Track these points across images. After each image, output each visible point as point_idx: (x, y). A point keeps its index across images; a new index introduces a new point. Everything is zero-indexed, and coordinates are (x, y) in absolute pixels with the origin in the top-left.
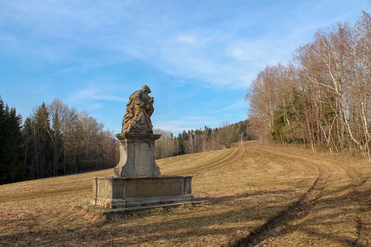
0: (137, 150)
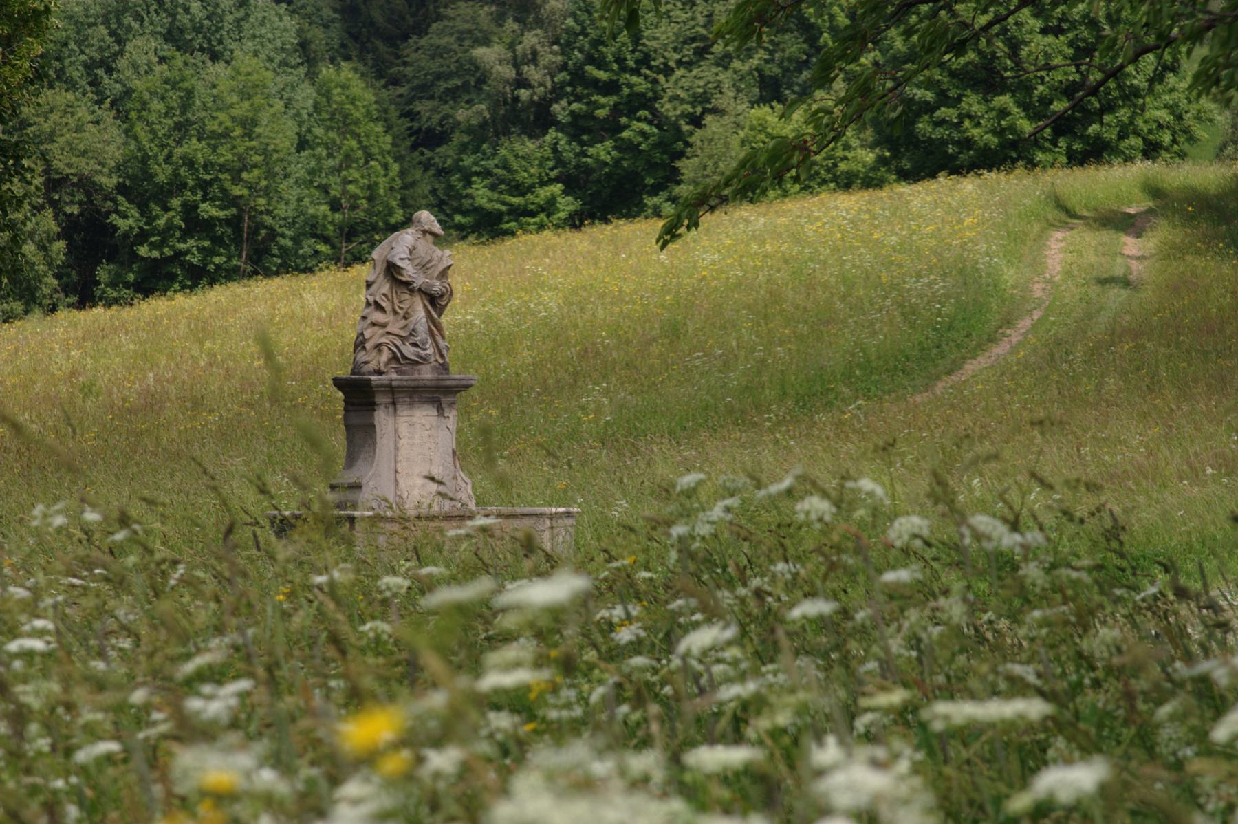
0: (403, 429)
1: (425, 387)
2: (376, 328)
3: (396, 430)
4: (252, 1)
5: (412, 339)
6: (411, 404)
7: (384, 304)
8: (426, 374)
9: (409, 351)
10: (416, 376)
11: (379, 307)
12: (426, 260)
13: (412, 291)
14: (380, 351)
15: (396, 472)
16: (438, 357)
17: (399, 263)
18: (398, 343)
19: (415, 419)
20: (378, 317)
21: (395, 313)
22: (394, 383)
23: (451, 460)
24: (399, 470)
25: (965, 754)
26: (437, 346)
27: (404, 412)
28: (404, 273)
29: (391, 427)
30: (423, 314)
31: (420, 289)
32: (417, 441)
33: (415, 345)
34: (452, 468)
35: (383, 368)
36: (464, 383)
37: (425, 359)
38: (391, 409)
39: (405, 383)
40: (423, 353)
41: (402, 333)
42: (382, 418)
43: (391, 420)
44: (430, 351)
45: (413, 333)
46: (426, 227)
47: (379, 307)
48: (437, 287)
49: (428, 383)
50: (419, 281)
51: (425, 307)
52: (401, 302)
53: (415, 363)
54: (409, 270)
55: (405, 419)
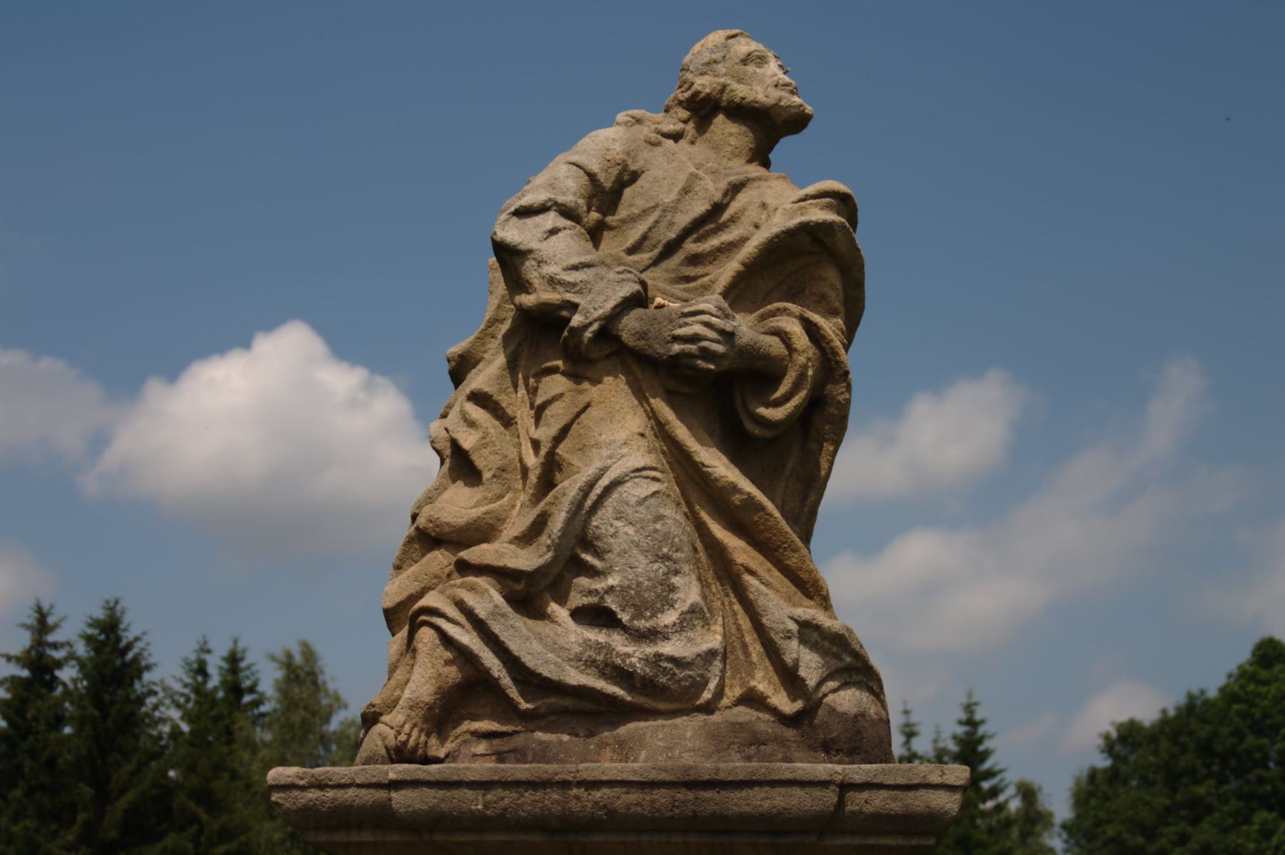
5: (582, 589)
9: (556, 645)
16: (764, 681)
18: (487, 599)
22: (401, 800)
40: (633, 654)
45: (577, 552)
46: (704, 84)
53: (589, 711)
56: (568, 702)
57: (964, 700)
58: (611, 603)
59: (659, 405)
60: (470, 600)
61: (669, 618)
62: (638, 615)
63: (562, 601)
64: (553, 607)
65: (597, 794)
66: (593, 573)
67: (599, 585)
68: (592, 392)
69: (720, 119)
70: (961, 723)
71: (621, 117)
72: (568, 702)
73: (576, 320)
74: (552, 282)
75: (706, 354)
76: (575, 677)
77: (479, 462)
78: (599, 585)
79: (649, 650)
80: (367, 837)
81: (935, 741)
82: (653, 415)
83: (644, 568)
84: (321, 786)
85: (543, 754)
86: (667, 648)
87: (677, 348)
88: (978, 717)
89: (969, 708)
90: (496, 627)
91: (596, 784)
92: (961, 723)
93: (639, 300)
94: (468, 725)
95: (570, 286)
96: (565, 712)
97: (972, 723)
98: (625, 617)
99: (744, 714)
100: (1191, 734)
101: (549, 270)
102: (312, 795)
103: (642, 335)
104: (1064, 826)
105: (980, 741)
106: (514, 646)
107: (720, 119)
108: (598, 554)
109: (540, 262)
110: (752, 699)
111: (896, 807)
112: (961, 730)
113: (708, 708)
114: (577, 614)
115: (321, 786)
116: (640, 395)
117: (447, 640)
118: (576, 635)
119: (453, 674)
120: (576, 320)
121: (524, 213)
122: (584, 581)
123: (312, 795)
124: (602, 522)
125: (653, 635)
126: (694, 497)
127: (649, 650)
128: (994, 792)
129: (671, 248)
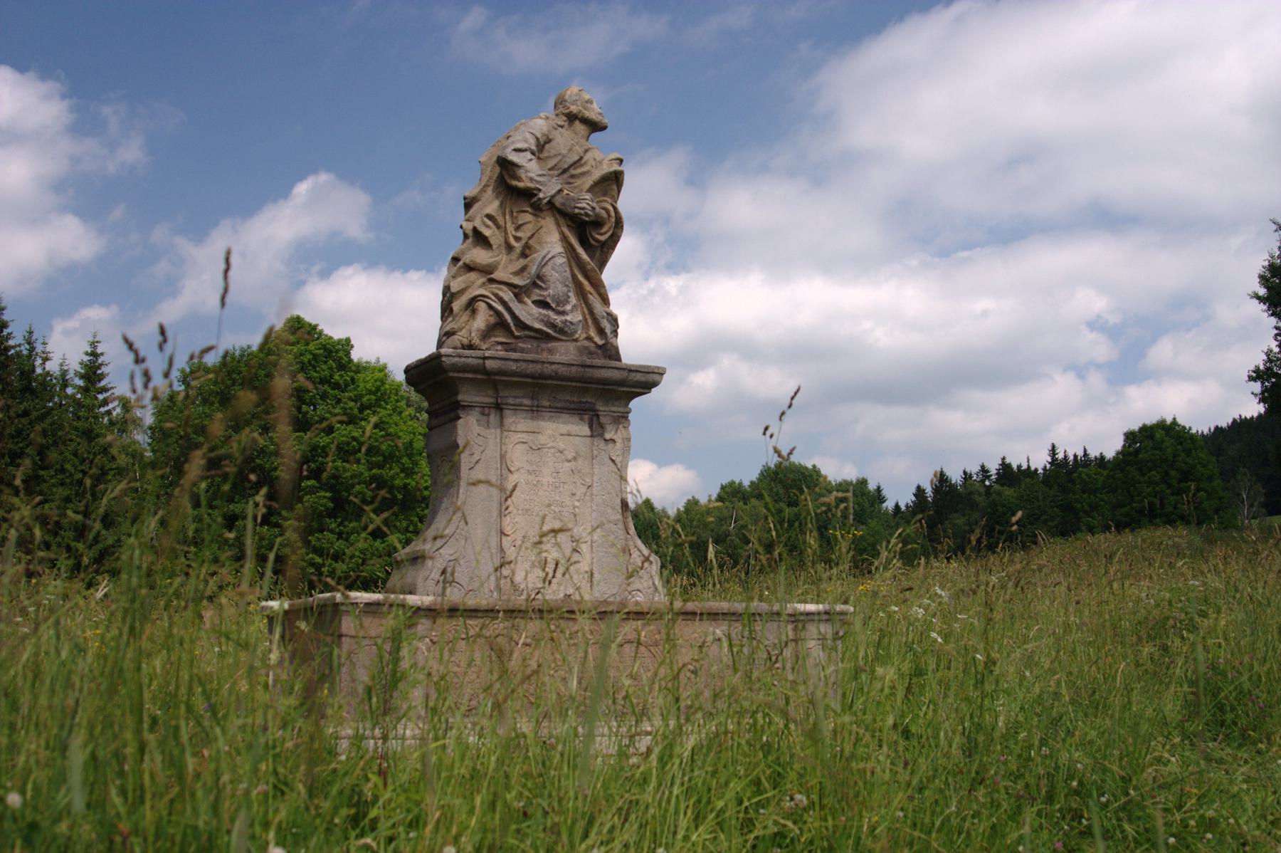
0: (518, 456)
1: (556, 377)
2: (473, 275)
3: (503, 457)
4: (1277, 520)
5: (537, 294)
6: (535, 411)
7: (487, 233)
8: (564, 354)
9: (529, 313)
10: (545, 356)
11: (480, 239)
12: (570, 161)
13: (537, 209)
14: (474, 312)
15: (502, 533)
16: (593, 333)
17: (514, 157)
18: (507, 295)
19: (542, 439)
20: (480, 256)
21: (510, 248)
22: (489, 363)
23: (619, 516)
24: (508, 530)
25: (514, 793)
26: (592, 313)
27: (519, 424)
28: (522, 173)
29: (492, 450)
30: (558, 248)
31: (550, 203)
32: (547, 478)
33: (543, 304)
34: (621, 533)
35: (476, 341)
36: (639, 377)
37: (563, 332)
38: (493, 418)
39: (513, 366)
40: (558, 319)
41: (517, 281)
42: (470, 428)
43: (492, 434)
44: (575, 317)
45: (538, 281)
46: (574, 109)
47: (480, 239)
48: (586, 203)
49: (563, 370)
50: (549, 188)
51: (564, 239)
52: (518, 228)
53: (542, 336)
54: (531, 171)
55: (524, 437)
56: (532, 334)
57: (91, 339)
58: (548, 300)
59: (566, 230)
60: (501, 294)
61: (568, 307)
62: (558, 305)
63: (529, 297)
64: (526, 299)
65: (553, 367)
66: (540, 288)
67: (545, 293)
68: (543, 222)
69: (577, 122)
70: (87, 354)
71: (542, 115)
72: (532, 334)
73: (541, 195)
74: (531, 179)
75: (587, 215)
76: (537, 326)
77: (492, 242)
78: (545, 293)
79: (563, 318)
80: (470, 376)
81: (61, 365)
82: (562, 233)
83: (561, 289)
84: (460, 356)
85: (522, 350)
86: (569, 318)
87: (577, 211)
88: (99, 351)
89: (93, 344)
90: (511, 305)
91: (553, 363)
92: (87, 354)
93: (560, 191)
94: (493, 339)
95: (538, 182)
96: (531, 337)
97: (94, 355)
98: (553, 306)
99: (587, 343)
100: (240, 373)
101: (531, 175)
102: (457, 359)
103: (563, 204)
104: (150, 428)
105: (99, 367)
106: (517, 312)
107: (577, 122)
108: (543, 282)
109: (527, 171)
110: (589, 339)
111: (643, 379)
112: (86, 358)
113: (576, 340)
114: (534, 302)
115: (460, 356)
116: (558, 225)
117: (490, 307)
118: (536, 311)
119: (492, 320)
120: (541, 195)
121: (517, 150)
122: (537, 291)
123: (457, 359)
124: (547, 271)
125: (563, 313)
126: (573, 264)
127: (563, 318)
128: (105, 402)
129: (565, 171)
